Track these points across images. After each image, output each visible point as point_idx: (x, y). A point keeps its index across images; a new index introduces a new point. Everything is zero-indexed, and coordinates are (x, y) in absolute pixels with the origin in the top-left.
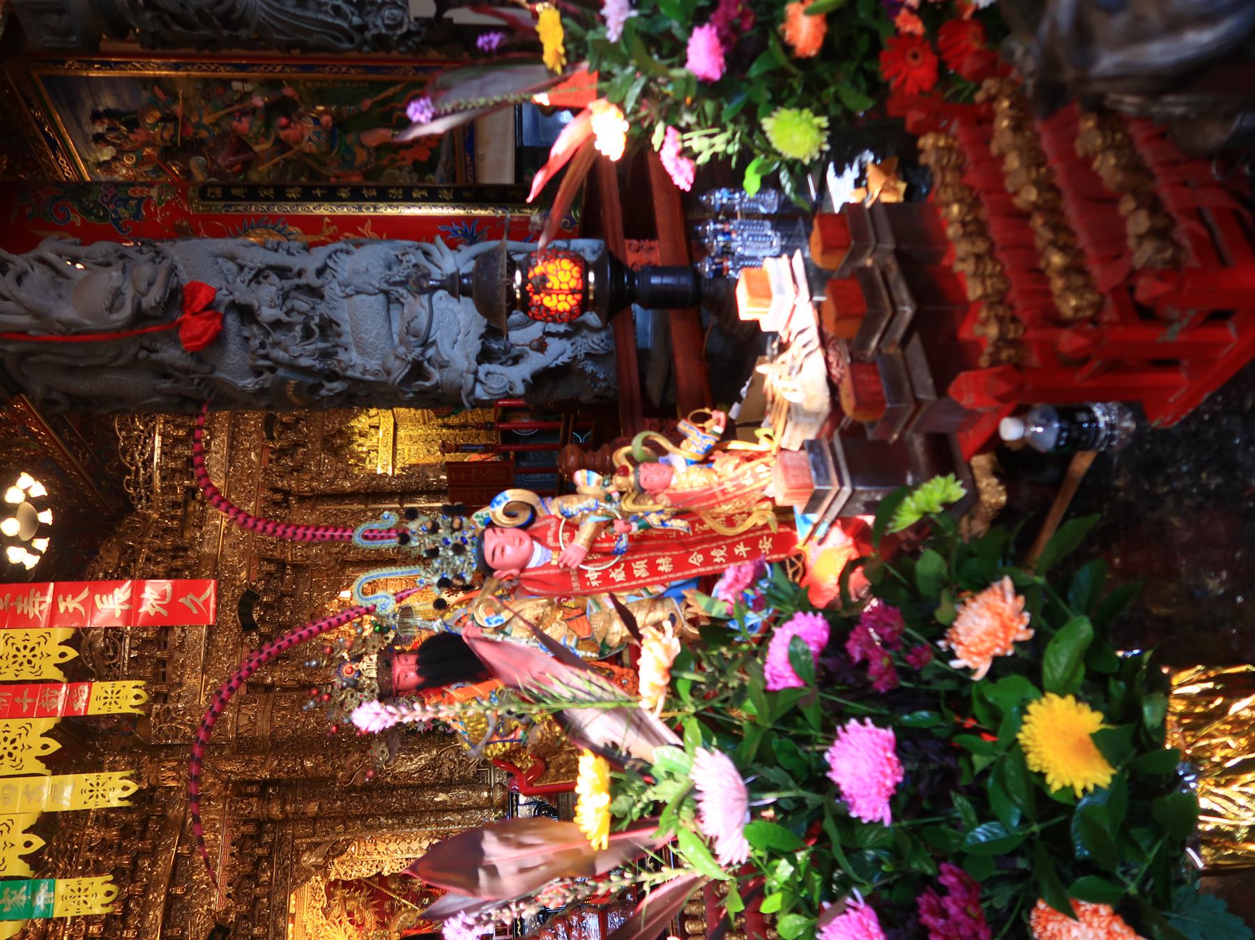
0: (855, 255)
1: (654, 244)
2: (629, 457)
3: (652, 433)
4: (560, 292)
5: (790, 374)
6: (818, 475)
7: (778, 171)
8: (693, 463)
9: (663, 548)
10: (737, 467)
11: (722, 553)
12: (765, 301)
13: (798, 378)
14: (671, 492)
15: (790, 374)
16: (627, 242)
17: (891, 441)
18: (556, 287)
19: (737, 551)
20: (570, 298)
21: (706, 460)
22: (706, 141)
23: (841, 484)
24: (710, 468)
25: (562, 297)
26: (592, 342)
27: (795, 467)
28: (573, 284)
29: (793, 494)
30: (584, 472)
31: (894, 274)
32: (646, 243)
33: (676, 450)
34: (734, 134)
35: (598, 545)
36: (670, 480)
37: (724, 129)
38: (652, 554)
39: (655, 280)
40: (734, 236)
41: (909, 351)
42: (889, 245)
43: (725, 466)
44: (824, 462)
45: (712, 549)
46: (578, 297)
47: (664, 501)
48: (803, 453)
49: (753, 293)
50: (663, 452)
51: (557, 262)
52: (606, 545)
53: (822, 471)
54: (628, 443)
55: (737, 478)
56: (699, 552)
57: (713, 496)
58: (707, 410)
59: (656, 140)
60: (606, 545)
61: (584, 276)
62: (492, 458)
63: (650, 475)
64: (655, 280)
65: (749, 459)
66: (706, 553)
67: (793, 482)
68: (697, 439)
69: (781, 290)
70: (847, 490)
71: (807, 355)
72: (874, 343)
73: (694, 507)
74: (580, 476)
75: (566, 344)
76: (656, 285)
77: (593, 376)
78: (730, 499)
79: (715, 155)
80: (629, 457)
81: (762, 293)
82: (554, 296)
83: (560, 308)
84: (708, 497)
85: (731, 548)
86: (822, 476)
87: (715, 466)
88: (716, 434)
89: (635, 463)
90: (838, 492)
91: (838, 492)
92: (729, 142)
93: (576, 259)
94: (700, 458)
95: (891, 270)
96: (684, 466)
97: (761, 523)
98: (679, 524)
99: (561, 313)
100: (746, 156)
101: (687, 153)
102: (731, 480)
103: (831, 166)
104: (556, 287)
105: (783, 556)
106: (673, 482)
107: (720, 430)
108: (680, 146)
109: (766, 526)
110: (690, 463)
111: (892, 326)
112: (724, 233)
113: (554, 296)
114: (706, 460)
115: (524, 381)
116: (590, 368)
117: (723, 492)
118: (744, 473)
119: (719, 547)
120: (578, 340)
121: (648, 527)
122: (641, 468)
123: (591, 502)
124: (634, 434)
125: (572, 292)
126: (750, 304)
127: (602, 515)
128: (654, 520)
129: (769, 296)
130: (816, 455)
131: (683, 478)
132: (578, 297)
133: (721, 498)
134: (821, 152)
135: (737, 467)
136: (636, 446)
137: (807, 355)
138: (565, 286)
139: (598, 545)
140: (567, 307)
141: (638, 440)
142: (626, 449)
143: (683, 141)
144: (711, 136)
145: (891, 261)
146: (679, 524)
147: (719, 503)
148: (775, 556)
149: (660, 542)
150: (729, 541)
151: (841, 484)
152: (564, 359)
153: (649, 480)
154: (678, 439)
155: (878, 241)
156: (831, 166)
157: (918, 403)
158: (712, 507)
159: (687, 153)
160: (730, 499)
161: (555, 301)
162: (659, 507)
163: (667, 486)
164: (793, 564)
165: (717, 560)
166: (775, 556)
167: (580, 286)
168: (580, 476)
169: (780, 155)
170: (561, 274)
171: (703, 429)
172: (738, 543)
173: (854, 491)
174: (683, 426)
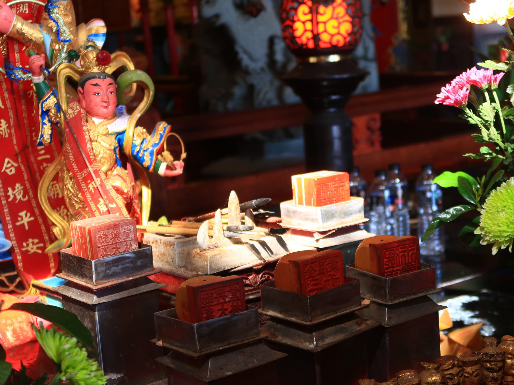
0: (377, 287)
1: (377, 146)
2: (122, 70)
3: (152, 93)
4: (315, 22)
5: (229, 229)
6: (108, 264)
7: (463, 202)
8: (120, 142)
9: (19, 126)
10: (118, 190)
11: (19, 197)
12: (314, 199)
13: (228, 240)
14: (84, 117)
15: (229, 229)
16: (377, 116)
17: (154, 340)
18: (321, 18)
19: (23, 214)
20: (309, 35)
21: (124, 158)
22: (490, 117)
23: (100, 293)
24: (116, 162)
25: (309, 26)
26: (267, 91)
27: (117, 237)
28: (325, 37)
29: (84, 238)
30: (104, 30)
31: (354, 328)
32: (377, 137)
33: (134, 122)
34: (502, 152)
35: (16, 48)
36: (97, 116)
37: (505, 139)
38: (11, 114)
39: (336, 131)
40: (390, 208)
41: (264, 347)
42: (387, 320)
43: (120, 179)
44: (125, 271)
45: (23, 184)
46: (311, 44)
47: (71, 110)
48: (135, 247)
49: (321, 183)
50: (130, 111)
51: (347, 18)
52: (17, 57)
53: (114, 269)
54: (137, 67)
55: (107, 192)
56: (18, 169)
57: (83, 166)
58: (184, 155)
59: (490, 65)
60: (17, 57)
61: (334, 49)
62: (135, 19)
63: (101, 93)
64: (336, 131)
65: (129, 206)
66: (17, 177)
67: (92, 230)
68: (150, 145)
69: (327, 216)
70: (94, 300)
71: (253, 247)
72: (271, 313)
73: (68, 147)
74: (99, 26)
75: (262, 62)
76: (329, 132)
77: (229, 96)
78: (80, 189)
79: (475, 128)
80: (122, 70)
81: (322, 197)
82: (309, 17)
83: (298, 26)
84: (81, 161)
85: (27, 206)
86: (110, 268)
87: (119, 170)
88: (156, 168)
89: (116, 75)
90: (89, 290)
91: (89, 290)
92: (492, 145)
93: (355, 39)
94: (127, 151)
95: (359, 324)
96: (116, 135)
97: (56, 231)
98: (46, 131)
99: (291, 27)
100: (477, 168)
101: (477, 94)
102: (102, 185)
103: (475, 298)
104: (321, 18)
105: (20, 266)
106: (96, 120)
107: (162, 170)
108: (485, 86)
109: (53, 239)
110: (120, 136)
111: (293, 331)
112: (393, 197)
113: (309, 17)
114: (124, 158)
115: (217, 16)
116: (238, 91)
117: (89, 178)
118: (112, 201)
119: (26, 193)
120: (268, 77)
121: (40, 96)
122: (109, 80)
123: (67, 34)
124: (148, 71)
125: (316, 37)
126: (309, 182)
127: (53, 50)
128: (50, 102)
129: (319, 203)
130: (133, 261)
131: (102, 130)
132: (311, 44)
133: (80, 176)
134: (490, 246)
135: (118, 190)
136: (135, 75)
137: (253, 247)
138: (321, 28)
139: (16, 48)
140: (298, 33)
141: (143, 76)
142: (131, 66)
143: (490, 91)
144: (497, 125)
145: (371, 323)
146: (46, 131)
147: (74, 177)
148: (19, 258)
149: (26, 122)
150: (34, 202)
151: (100, 293)
152: (245, 60)
153: (96, 89)
154: (147, 123)
155: (391, 307)
156: (475, 298)
157: (200, 362)
158: (70, 169)
159: (477, 94)
160: (80, 189)
161: (303, 18)
162: (64, 107)
163: (90, 113)
164: (11, 279)
165: (10, 192)
166: (19, 258)
167: (322, 45)
168: (99, 26)
169: (482, 201)
170: (334, 23)
171: (160, 152)
172: (33, 214)
173: (92, 308)
174: (163, 128)
